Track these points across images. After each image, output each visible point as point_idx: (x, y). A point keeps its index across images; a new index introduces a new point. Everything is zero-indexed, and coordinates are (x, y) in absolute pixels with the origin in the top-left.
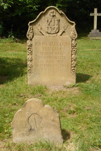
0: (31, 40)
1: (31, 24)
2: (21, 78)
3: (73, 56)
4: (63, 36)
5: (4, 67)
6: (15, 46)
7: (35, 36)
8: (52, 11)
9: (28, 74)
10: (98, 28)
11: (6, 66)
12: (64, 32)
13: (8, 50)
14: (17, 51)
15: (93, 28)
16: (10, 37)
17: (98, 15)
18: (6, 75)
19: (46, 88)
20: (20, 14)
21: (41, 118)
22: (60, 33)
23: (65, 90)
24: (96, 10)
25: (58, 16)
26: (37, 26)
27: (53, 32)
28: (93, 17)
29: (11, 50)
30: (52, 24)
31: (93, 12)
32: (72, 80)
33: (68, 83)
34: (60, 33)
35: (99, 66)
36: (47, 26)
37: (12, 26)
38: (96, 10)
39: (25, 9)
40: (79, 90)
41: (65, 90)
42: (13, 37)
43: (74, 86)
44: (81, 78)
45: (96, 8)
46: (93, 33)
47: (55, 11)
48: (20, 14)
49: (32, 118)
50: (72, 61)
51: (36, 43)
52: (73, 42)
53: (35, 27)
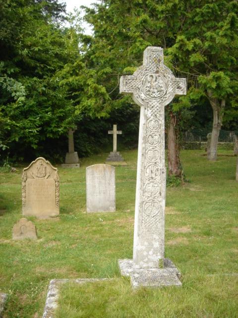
0: (25, 182)
1: (25, 170)
2: (17, 211)
3: (57, 194)
4: (48, 179)
5: (2, 202)
6: (11, 177)
7: (28, 179)
8: (41, 161)
9: (23, 208)
10: (118, 150)
11: (4, 201)
12: (49, 176)
13: (3, 183)
14: (14, 183)
15: (112, 150)
16: (5, 166)
17: (118, 133)
18: (4, 209)
19: (36, 218)
20: (17, 140)
21: (26, 227)
22: (46, 177)
23: (49, 218)
24: (115, 127)
25: (45, 164)
26: (30, 171)
27: (42, 175)
28: (112, 136)
29: (6, 182)
30: (41, 170)
31: (112, 129)
32: (56, 212)
33: (53, 214)
34: (46, 177)
35: (236, 188)
36: (37, 171)
37: (9, 153)
38: (115, 127)
39: (23, 133)
40: (60, 218)
41: (49, 218)
42: (9, 166)
43: (58, 216)
44: (62, 210)
45: (115, 124)
46: (112, 157)
47: (42, 161)
48: (17, 140)
49: (22, 227)
50: (56, 197)
51: (29, 184)
52: (56, 183)
53: (27, 171)
